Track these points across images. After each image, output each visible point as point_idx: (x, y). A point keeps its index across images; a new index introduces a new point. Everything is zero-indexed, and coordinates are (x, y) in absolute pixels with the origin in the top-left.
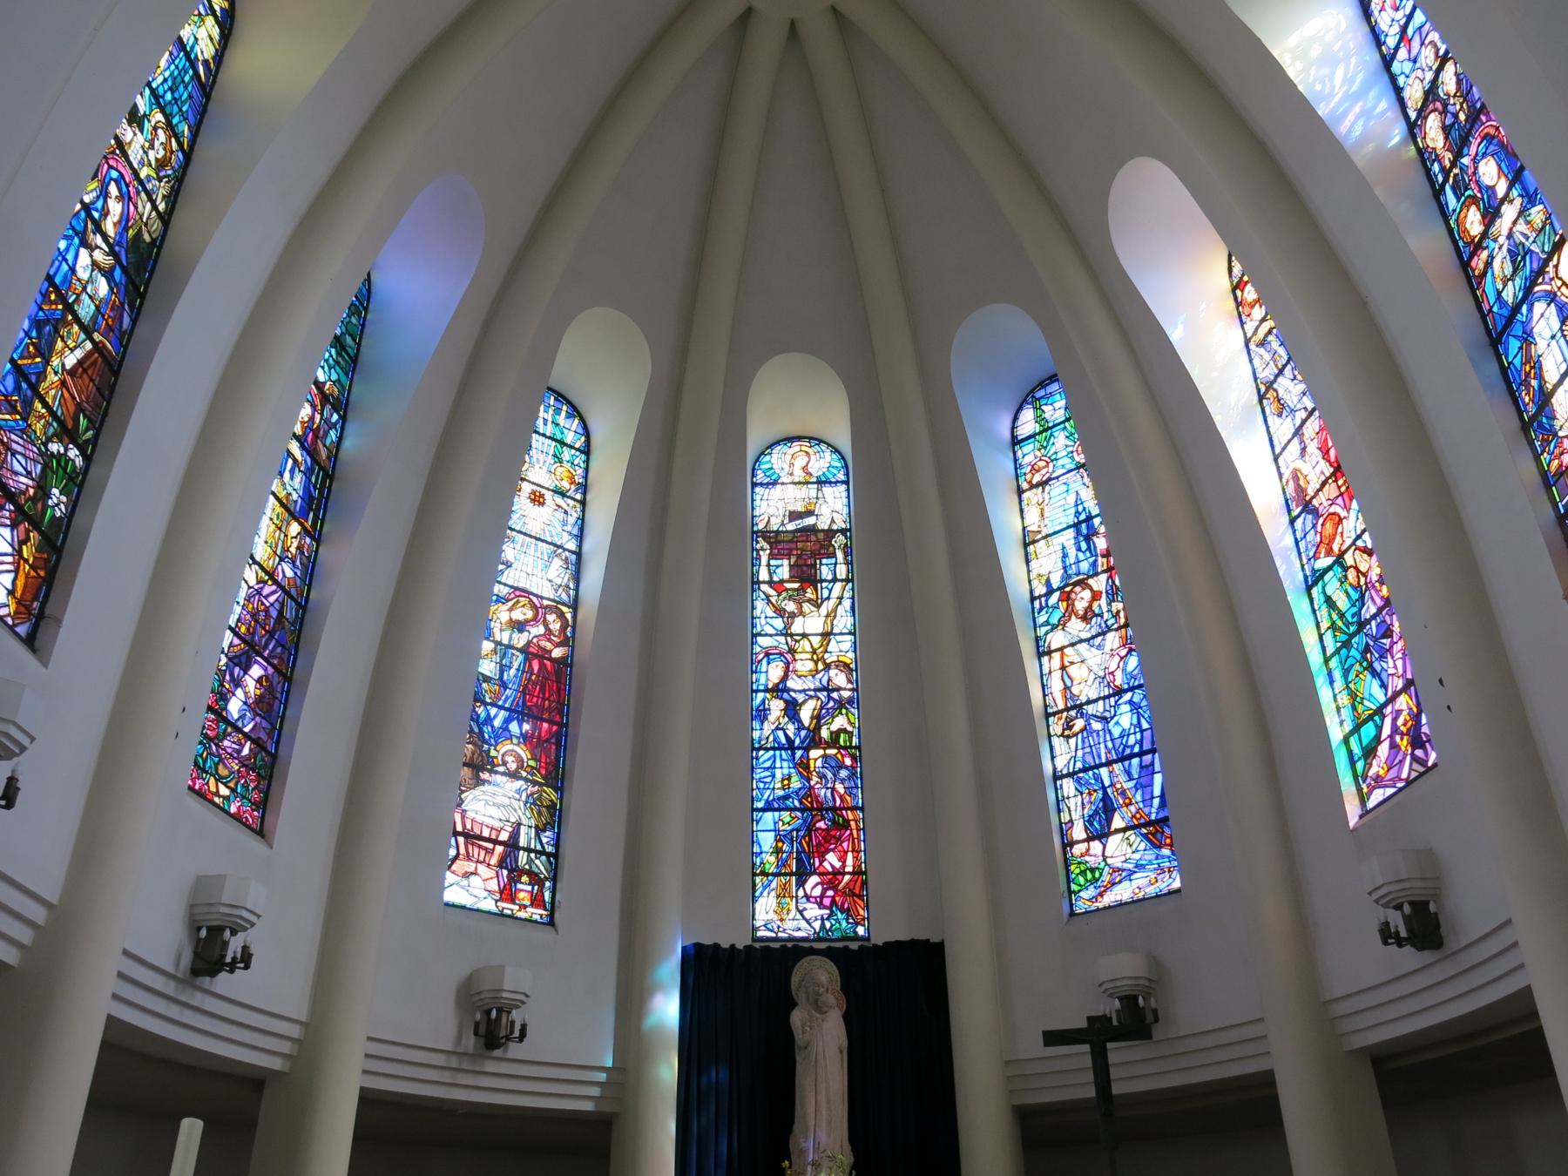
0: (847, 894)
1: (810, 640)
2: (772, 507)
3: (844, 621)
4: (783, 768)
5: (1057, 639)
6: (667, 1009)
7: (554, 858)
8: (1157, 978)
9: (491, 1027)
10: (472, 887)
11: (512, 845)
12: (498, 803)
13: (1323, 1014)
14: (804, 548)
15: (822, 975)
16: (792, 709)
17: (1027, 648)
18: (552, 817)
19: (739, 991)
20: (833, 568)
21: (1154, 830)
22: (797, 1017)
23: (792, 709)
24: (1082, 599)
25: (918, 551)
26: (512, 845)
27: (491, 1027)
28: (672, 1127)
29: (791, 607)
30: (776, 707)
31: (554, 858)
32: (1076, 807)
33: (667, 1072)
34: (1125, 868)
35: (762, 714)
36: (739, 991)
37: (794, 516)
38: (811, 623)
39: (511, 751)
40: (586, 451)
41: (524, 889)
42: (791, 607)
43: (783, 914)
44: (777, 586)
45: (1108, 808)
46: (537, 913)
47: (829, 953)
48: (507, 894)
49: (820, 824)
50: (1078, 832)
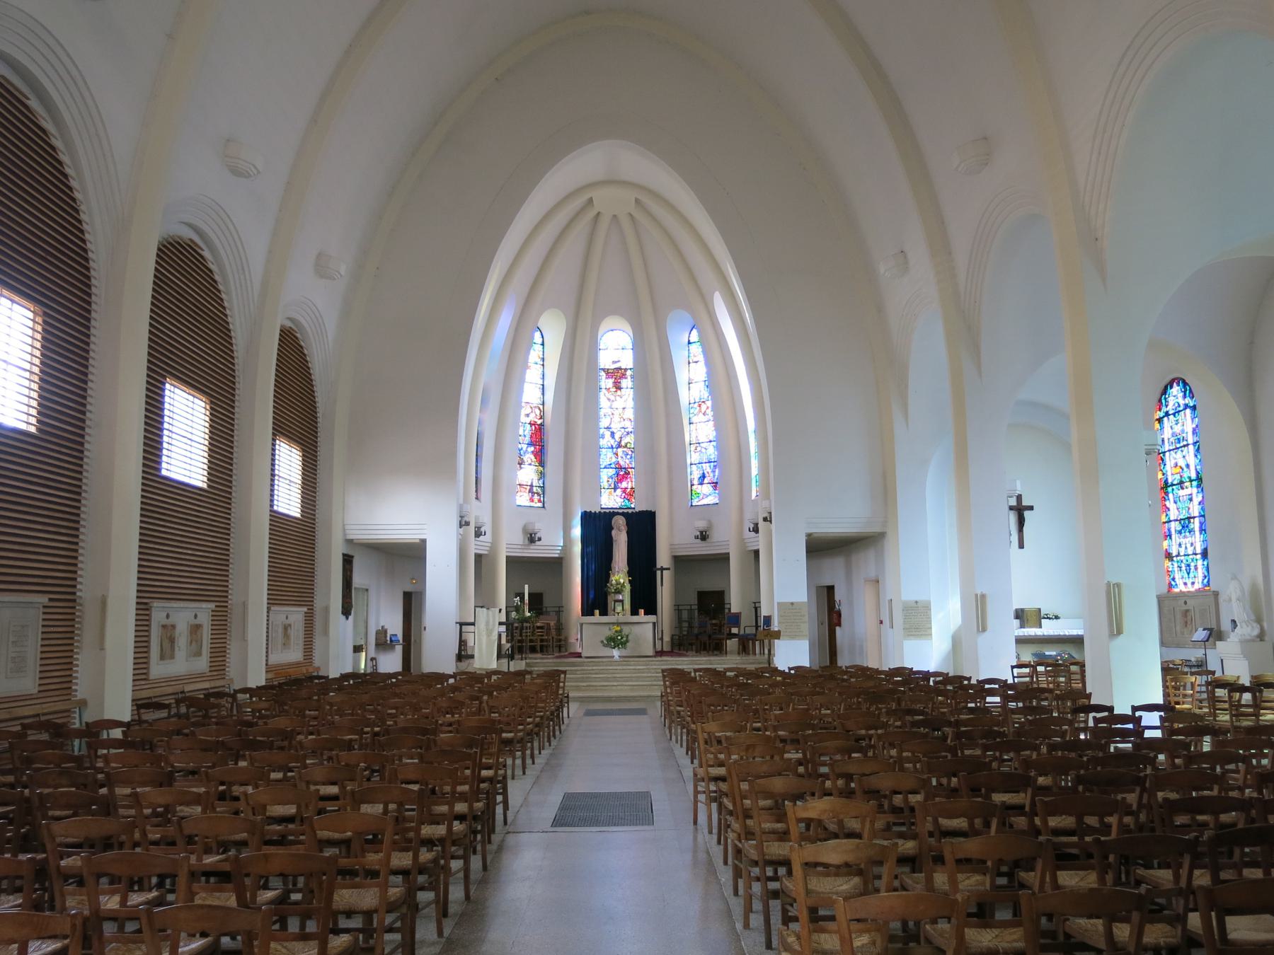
0: (629, 495)
1: (617, 410)
2: (605, 360)
3: (630, 404)
4: (610, 454)
5: (694, 420)
6: (577, 532)
7: (543, 488)
8: (710, 526)
9: (532, 538)
10: (523, 499)
11: (532, 486)
12: (528, 474)
13: (742, 541)
14: (617, 375)
15: (620, 522)
16: (613, 434)
17: (686, 422)
18: (542, 475)
19: (597, 526)
20: (627, 383)
21: (715, 485)
22: (613, 533)
23: (613, 434)
24: (704, 407)
25: (653, 379)
26: (532, 486)
27: (532, 538)
28: (579, 562)
29: (612, 398)
30: (608, 434)
31: (543, 488)
32: (696, 475)
33: (577, 548)
34: (706, 495)
35: (603, 436)
36: (597, 526)
37: (614, 362)
38: (619, 403)
39: (529, 457)
40: (543, 344)
41: (536, 497)
42: (612, 398)
43: (611, 500)
44: (608, 389)
45: (704, 476)
46: (540, 505)
47: (623, 514)
48: (532, 500)
49: (622, 474)
50: (696, 482)
